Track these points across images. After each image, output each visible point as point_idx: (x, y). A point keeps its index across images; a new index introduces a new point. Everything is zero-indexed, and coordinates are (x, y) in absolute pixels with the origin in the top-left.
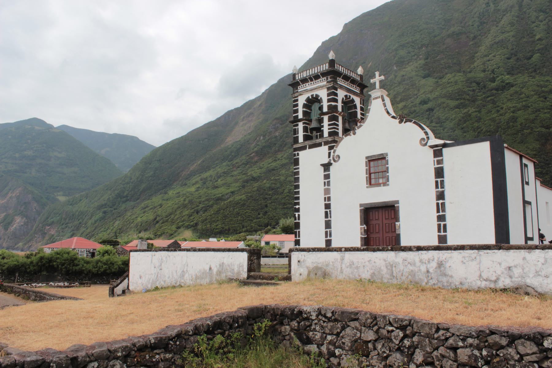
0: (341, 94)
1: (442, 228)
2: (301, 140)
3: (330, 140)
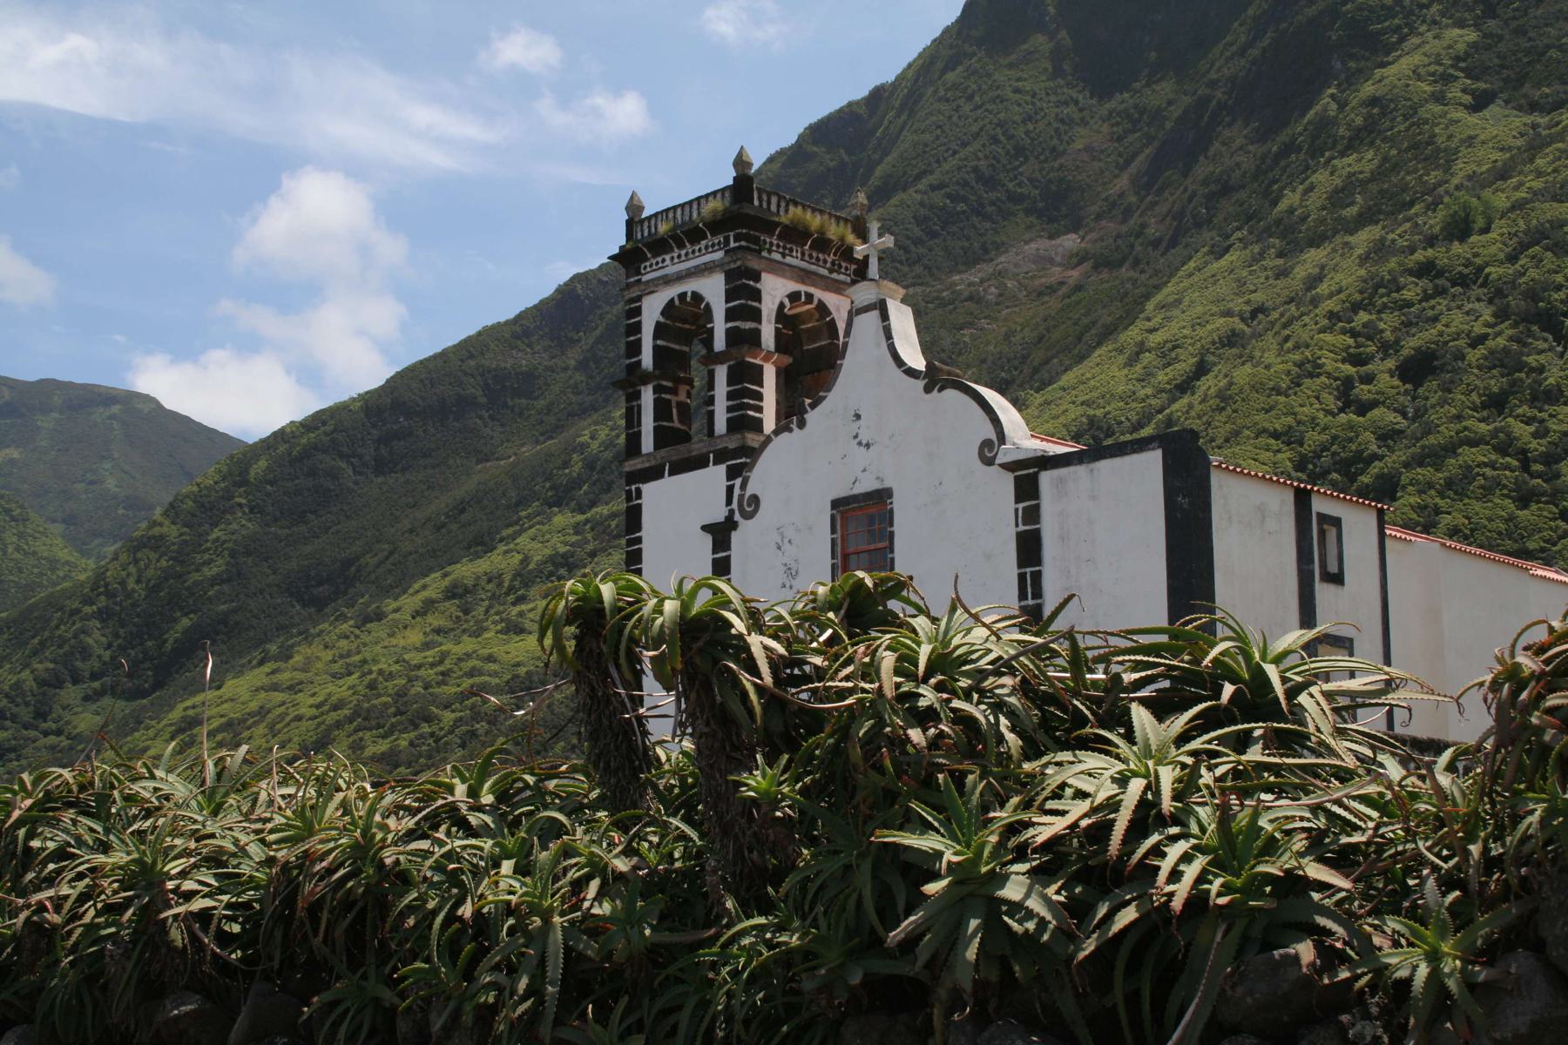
0: (774, 290)
2: (647, 444)
3: (732, 446)
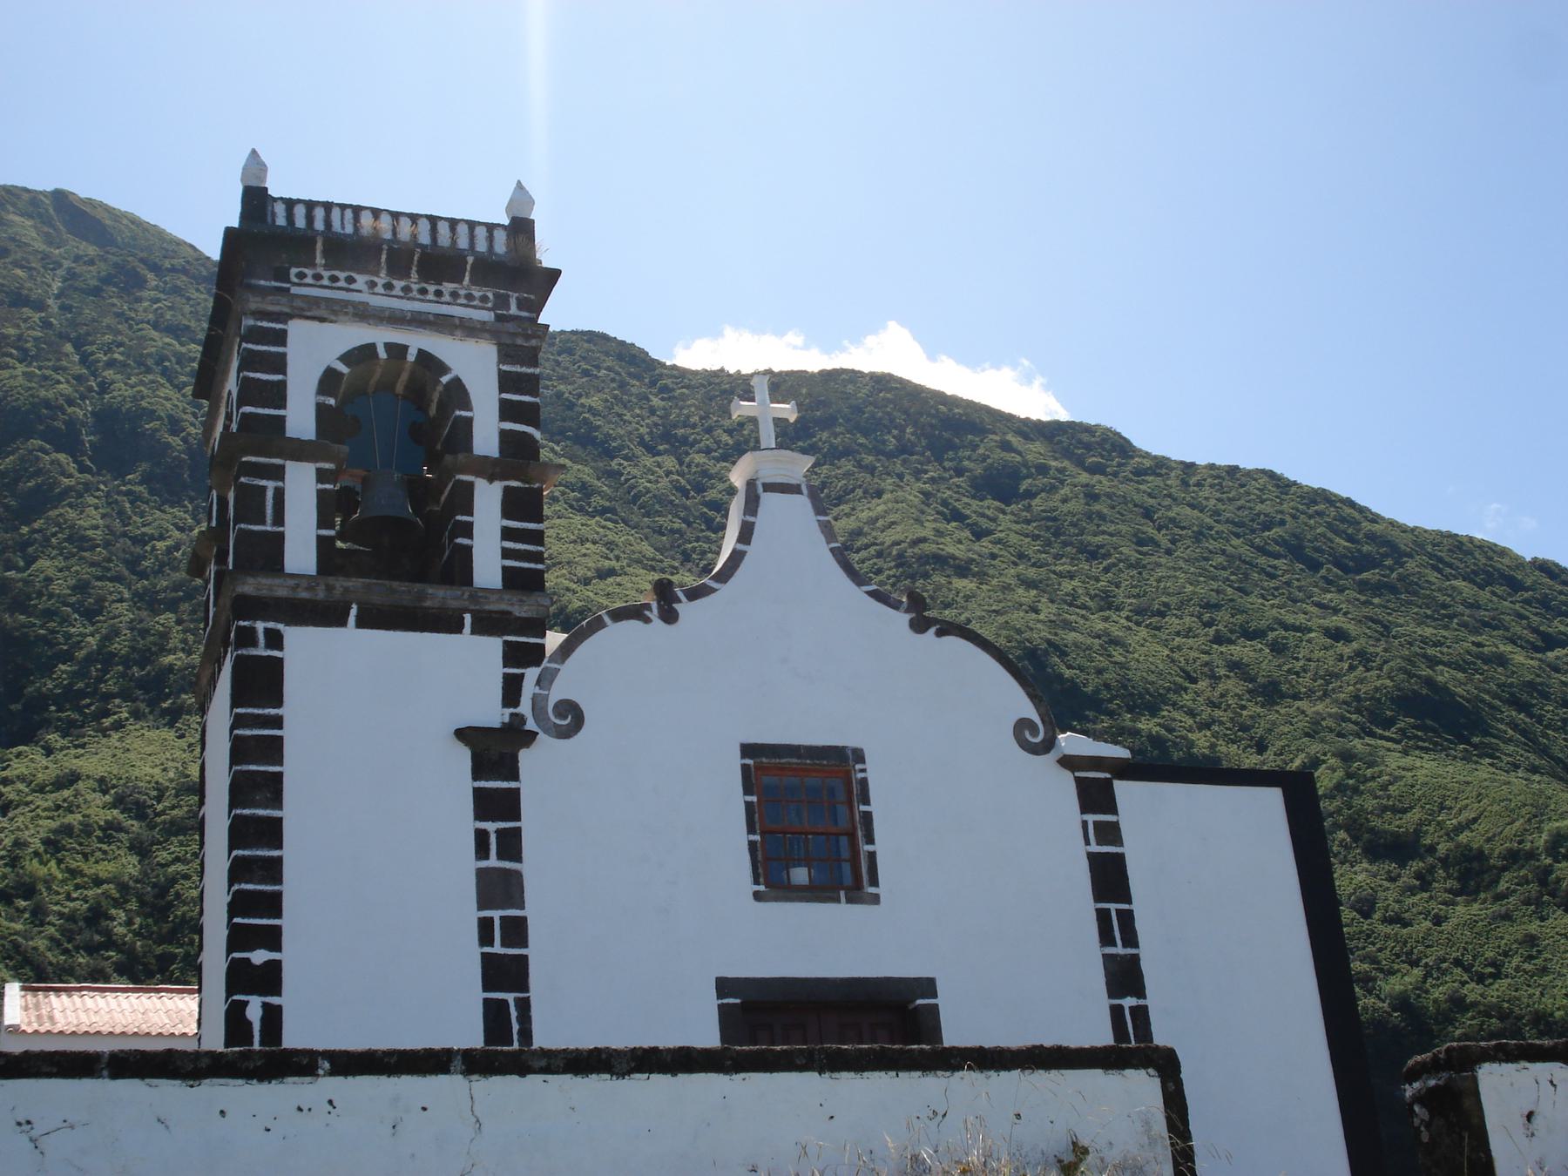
1: (505, 972)
